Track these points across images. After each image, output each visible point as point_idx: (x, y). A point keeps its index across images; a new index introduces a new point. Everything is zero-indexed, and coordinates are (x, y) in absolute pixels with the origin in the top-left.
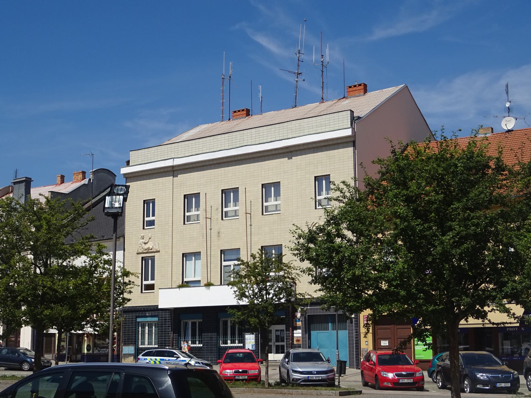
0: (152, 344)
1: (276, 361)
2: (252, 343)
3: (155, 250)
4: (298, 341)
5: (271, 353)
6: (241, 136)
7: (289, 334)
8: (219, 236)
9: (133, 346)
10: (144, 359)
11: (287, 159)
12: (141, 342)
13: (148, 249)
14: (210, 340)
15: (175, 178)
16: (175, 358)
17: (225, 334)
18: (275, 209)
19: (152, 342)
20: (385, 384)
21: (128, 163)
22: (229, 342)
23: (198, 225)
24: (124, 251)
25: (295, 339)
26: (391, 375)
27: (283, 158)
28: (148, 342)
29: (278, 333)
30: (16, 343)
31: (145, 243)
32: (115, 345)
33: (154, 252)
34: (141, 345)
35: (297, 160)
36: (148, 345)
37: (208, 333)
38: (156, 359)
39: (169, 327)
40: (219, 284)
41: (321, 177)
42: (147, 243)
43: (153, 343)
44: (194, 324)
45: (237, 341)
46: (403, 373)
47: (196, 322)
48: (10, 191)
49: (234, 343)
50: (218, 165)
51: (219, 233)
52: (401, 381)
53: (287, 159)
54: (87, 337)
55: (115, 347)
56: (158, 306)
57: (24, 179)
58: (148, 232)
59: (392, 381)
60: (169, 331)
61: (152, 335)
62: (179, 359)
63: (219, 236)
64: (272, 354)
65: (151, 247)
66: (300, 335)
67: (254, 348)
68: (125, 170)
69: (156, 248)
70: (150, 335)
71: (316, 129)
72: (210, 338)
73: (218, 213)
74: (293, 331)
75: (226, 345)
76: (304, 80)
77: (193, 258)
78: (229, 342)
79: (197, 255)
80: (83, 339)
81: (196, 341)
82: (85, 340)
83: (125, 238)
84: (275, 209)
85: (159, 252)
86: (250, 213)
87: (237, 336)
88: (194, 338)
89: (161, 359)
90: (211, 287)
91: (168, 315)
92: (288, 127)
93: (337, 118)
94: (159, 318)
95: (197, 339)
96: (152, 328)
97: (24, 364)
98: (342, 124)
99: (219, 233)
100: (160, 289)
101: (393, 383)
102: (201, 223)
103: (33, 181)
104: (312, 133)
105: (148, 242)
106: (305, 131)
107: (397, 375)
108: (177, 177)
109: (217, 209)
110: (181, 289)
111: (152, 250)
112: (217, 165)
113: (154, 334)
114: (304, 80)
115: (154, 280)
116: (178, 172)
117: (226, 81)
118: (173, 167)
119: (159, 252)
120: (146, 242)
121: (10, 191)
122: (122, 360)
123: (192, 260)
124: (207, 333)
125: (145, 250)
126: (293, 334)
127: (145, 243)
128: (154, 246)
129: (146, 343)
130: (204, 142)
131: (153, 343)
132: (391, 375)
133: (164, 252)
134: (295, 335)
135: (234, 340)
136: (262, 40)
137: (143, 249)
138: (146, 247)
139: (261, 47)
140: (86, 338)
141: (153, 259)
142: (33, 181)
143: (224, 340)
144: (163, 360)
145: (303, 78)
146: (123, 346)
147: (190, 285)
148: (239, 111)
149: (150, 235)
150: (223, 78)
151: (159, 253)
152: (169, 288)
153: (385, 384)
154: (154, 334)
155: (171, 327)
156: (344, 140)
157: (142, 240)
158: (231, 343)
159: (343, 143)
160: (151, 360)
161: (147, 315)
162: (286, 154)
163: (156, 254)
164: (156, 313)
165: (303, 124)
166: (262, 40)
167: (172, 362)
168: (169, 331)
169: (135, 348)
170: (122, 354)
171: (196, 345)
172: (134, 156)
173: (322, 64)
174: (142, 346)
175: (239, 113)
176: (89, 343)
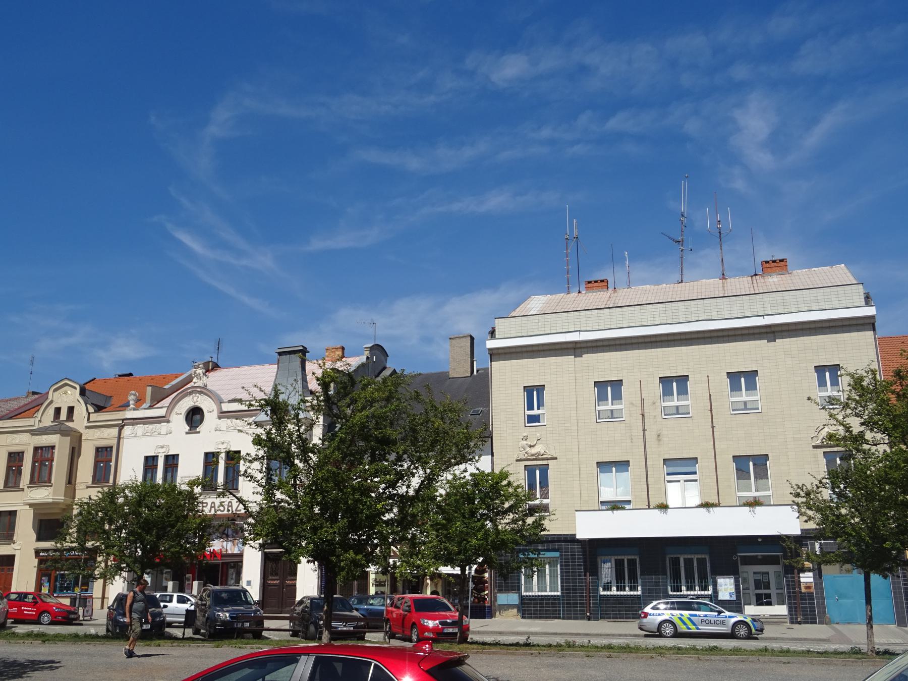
0: (546, 591)
1: (759, 615)
2: (729, 591)
3: (550, 456)
4: (808, 587)
5: (750, 604)
6: (686, 307)
7: (794, 578)
8: (659, 440)
9: (516, 593)
10: (659, 615)
11: (766, 341)
12: (526, 588)
13: (539, 454)
14: (656, 586)
15: (577, 359)
16: (716, 614)
17: (676, 577)
18: (743, 408)
19: (546, 587)
20: (426, 634)
21: (492, 333)
22: (684, 588)
23: (623, 424)
24: (493, 455)
25: (802, 586)
26: (431, 624)
27: (760, 339)
28: (538, 587)
29: (759, 577)
30: (283, 588)
31: (531, 446)
32: (486, 592)
33: (548, 459)
34: (526, 591)
35: (782, 343)
36: (538, 591)
37: (652, 575)
38: (682, 615)
39: (580, 565)
40: (645, 506)
41: (823, 368)
42: (533, 446)
43: (548, 589)
44: (689, 562)
45: (697, 588)
46: (448, 621)
47: (623, 560)
48: (210, 368)
49: (693, 589)
50: (673, 342)
51: (659, 436)
52: (446, 631)
53: (766, 341)
54: (431, 579)
55: (487, 595)
56: (575, 535)
57: (301, 348)
58: (533, 432)
59: (434, 630)
60: (581, 572)
61: (545, 577)
62: (722, 614)
63: (659, 440)
64: (752, 607)
65: (542, 452)
66: (811, 580)
67: (734, 598)
68: (491, 344)
69: (551, 453)
70: (542, 577)
71: (810, 305)
72: (656, 582)
73: (656, 409)
74: (799, 574)
75: (678, 593)
76: (691, 250)
77: (614, 469)
78: (684, 588)
79: (623, 465)
80: (423, 582)
81: (695, 586)
82: (427, 584)
83: (494, 438)
84: (743, 408)
85: (556, 458)
86: (117, 429)
87: (696, 581)
88: (691, 582)
89: (691, 615)
90: (758, 508)
91: (577, 549)
92: (765, 300)
93: (843, 292)
94: (561, 552)
95: (627, 584)
96: (557, 566)
97: (737, 633)
98: (851, 301)
99: (659, 436)
100: (577, 511)
101: (437, 633)
102: (626, 422)
103: (309, 352)
104: (804, 309)
105: (535, 445)
106: (792, 306)
107: (441, 623)
108: (582, 357)
109: (654, 403)
110: (615, 512)
111: (544, 456)
112: (650, 344)
113: (548, 577)
114: (691, 250)
115: (548, 498)
116: (583, 350)
117: (572, 244)
118: (576, 343)
119: (556, 458)
120: (532, 444)
121: (210, 368)
122: (495, 614)
123: (612, 472)
124: (648, 575)
125: (532, 455)
126: (799, 577)
127: (531, 446)
128: (547, 451)
129: (535, 588)
130: (623, 313)
131: (548, 589)
132: (431, 624)
133: (565, 460)
134: (802, 580)
135: (677, 586)
136: (185, 238)
137: (528, 454)
138: (533, 451)
139: (180, 243)
140: (429, 581)
141: (544, 470)
142: (309, 352)
143: (674, 585)
144: (696, 615)
145: (690, 247)
146: (498, 593)
147: (626, 506)
148: (596, 282)
149: (538, 435)
150: (567, 239)
151: (556, 461)
152: (737, 506)
153: (426, 634)
154: (548, 577)
155: (584, 565)
156: (862, 322)
157: (525, 442)
158: (688, 589)
159: (857, 325)
160: (673, 615)
161: (539, 548)
162: (765, 335)
163: (550, 462)
164: (549, 545)
165: (788, 297)
166: (185, 238)
167: (713, 619)
168: (581, 572)
169: (519, 595)
170: (496, 604)
171: (625, 593)
172: (501, 326)
173: (720, 232)
174: (528, 594)
175: (596, 284)
176: (434, 589)
